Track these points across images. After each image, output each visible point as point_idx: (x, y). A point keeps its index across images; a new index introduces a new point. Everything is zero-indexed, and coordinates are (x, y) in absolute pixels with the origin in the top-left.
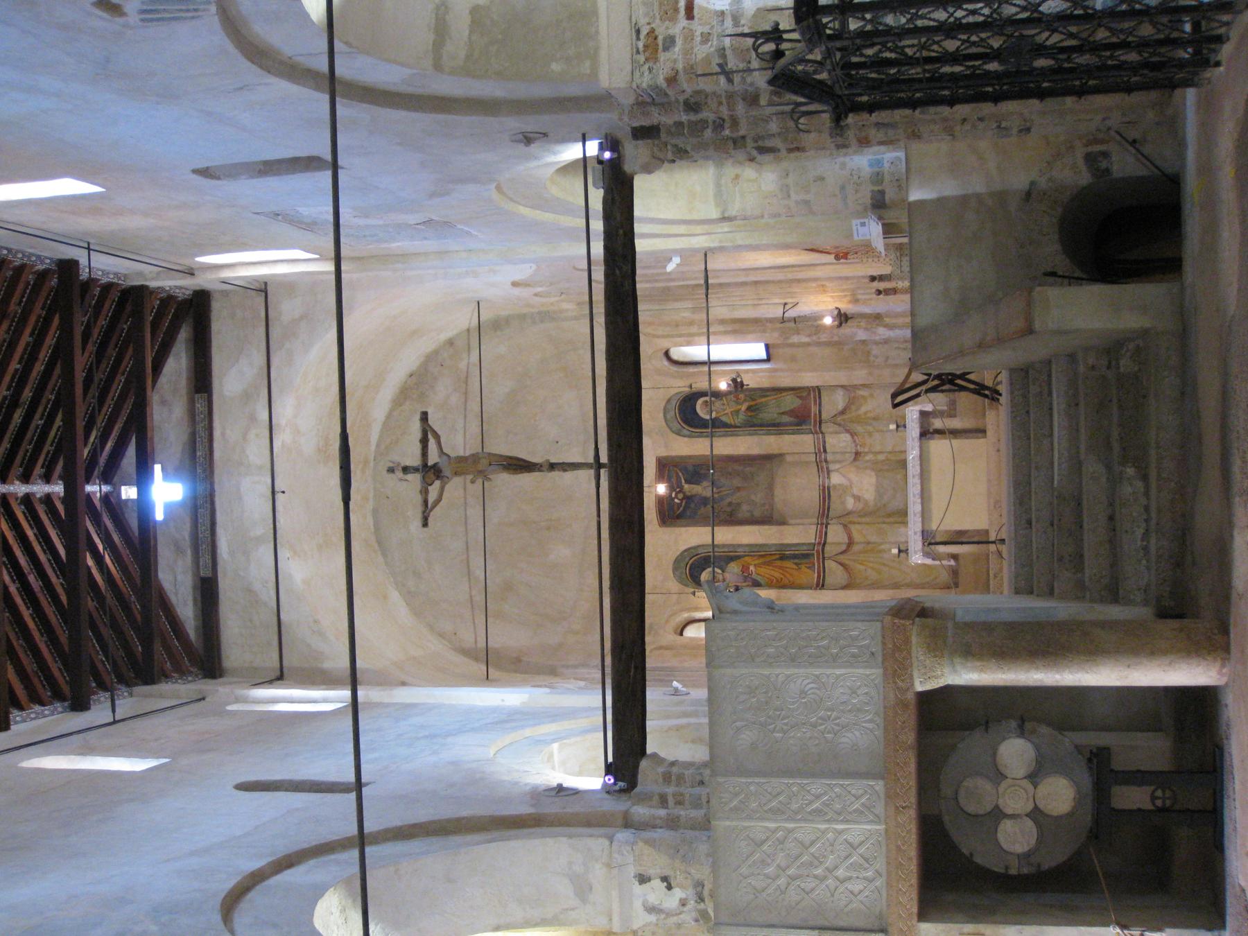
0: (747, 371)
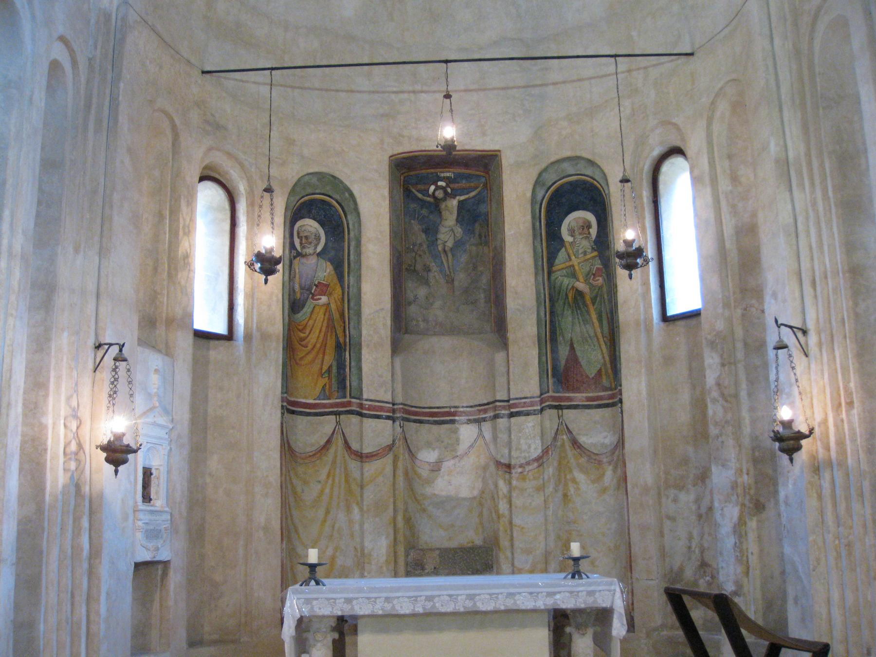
0: (646, 284)
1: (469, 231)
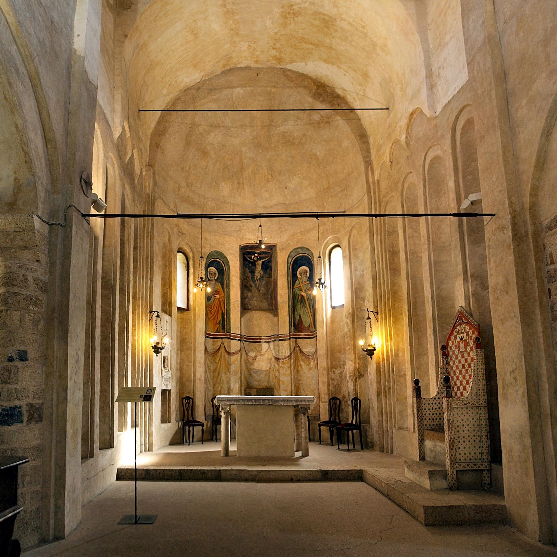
1: (265, 273)
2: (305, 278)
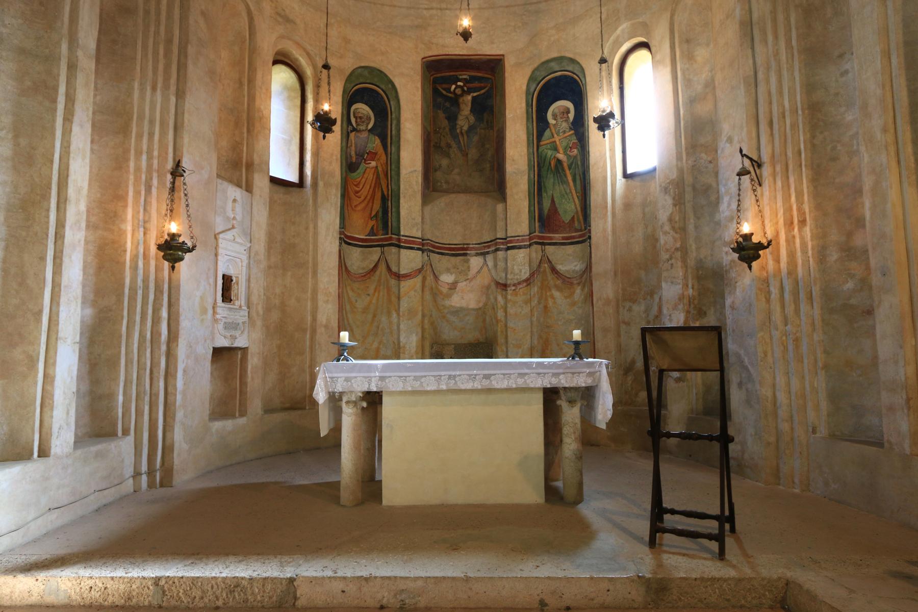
2: (564, 125)
